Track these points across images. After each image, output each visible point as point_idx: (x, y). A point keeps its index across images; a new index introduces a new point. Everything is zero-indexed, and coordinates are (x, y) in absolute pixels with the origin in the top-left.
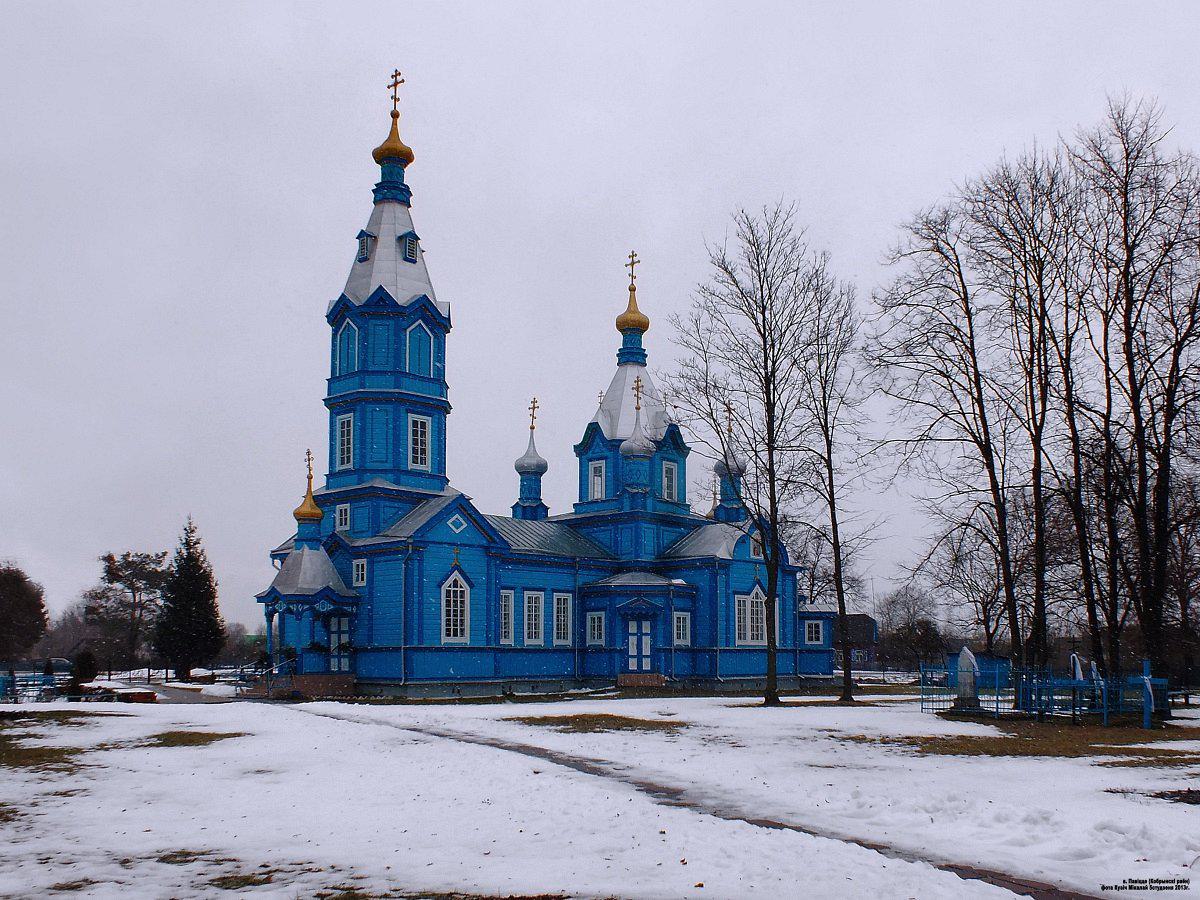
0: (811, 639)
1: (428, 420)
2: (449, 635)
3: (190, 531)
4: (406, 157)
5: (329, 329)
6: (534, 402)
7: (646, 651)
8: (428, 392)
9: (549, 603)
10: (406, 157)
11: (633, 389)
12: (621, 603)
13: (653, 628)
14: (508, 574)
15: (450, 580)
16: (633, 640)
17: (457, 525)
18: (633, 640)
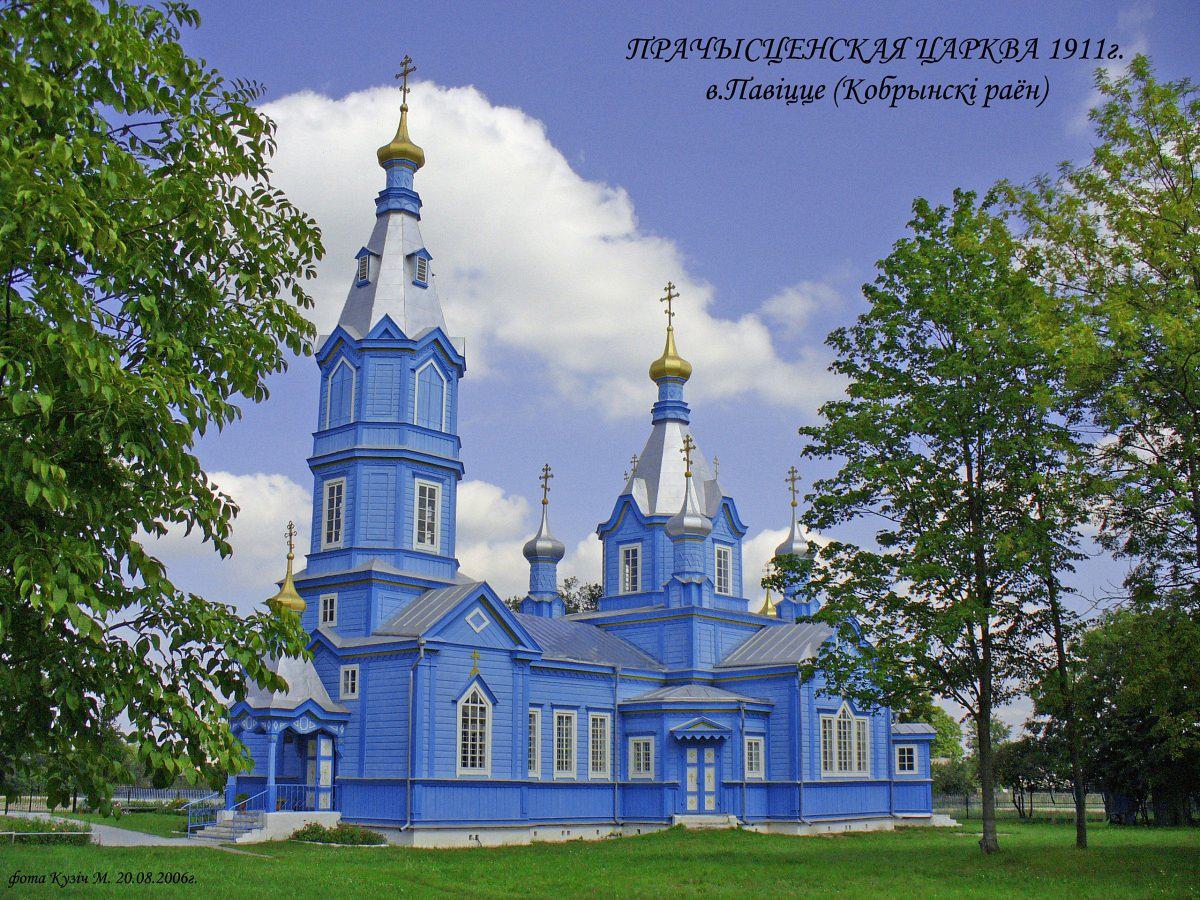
0: (902, 767)
1: (439, 488)
2: (465, 765)
3: (1074, 572)
4: (416, 161)
5: (318, 373)
6: (547, 469)
7: (710, 785)
8: (442, 450)
9: (547, 723)
10: (416, 161)
11: (681, 451)
12: (675, 725)
13: (717, 756)
14: (545, 689)
15: (468, 694)
16: (692, 772)
17: (478, 623)
18: (692, 772)
